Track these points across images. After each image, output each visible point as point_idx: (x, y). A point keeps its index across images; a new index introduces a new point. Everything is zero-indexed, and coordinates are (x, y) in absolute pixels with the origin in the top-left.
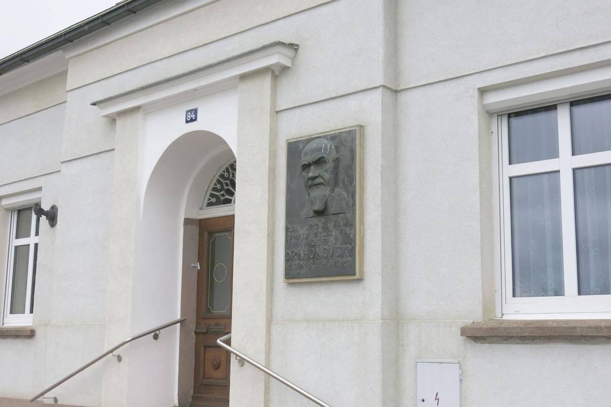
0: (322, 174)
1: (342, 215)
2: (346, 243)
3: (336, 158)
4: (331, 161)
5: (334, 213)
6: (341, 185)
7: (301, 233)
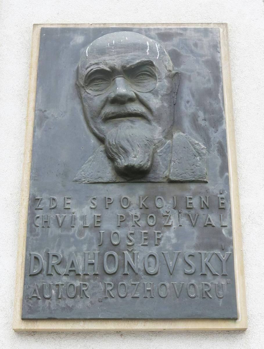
0: (144, 96)
1: (193, 187)
2: (211, 247)
3: (174, 72)
4: (163, 75)
5: (173, 178)
6: (186, 123)
7: (78, 215)
